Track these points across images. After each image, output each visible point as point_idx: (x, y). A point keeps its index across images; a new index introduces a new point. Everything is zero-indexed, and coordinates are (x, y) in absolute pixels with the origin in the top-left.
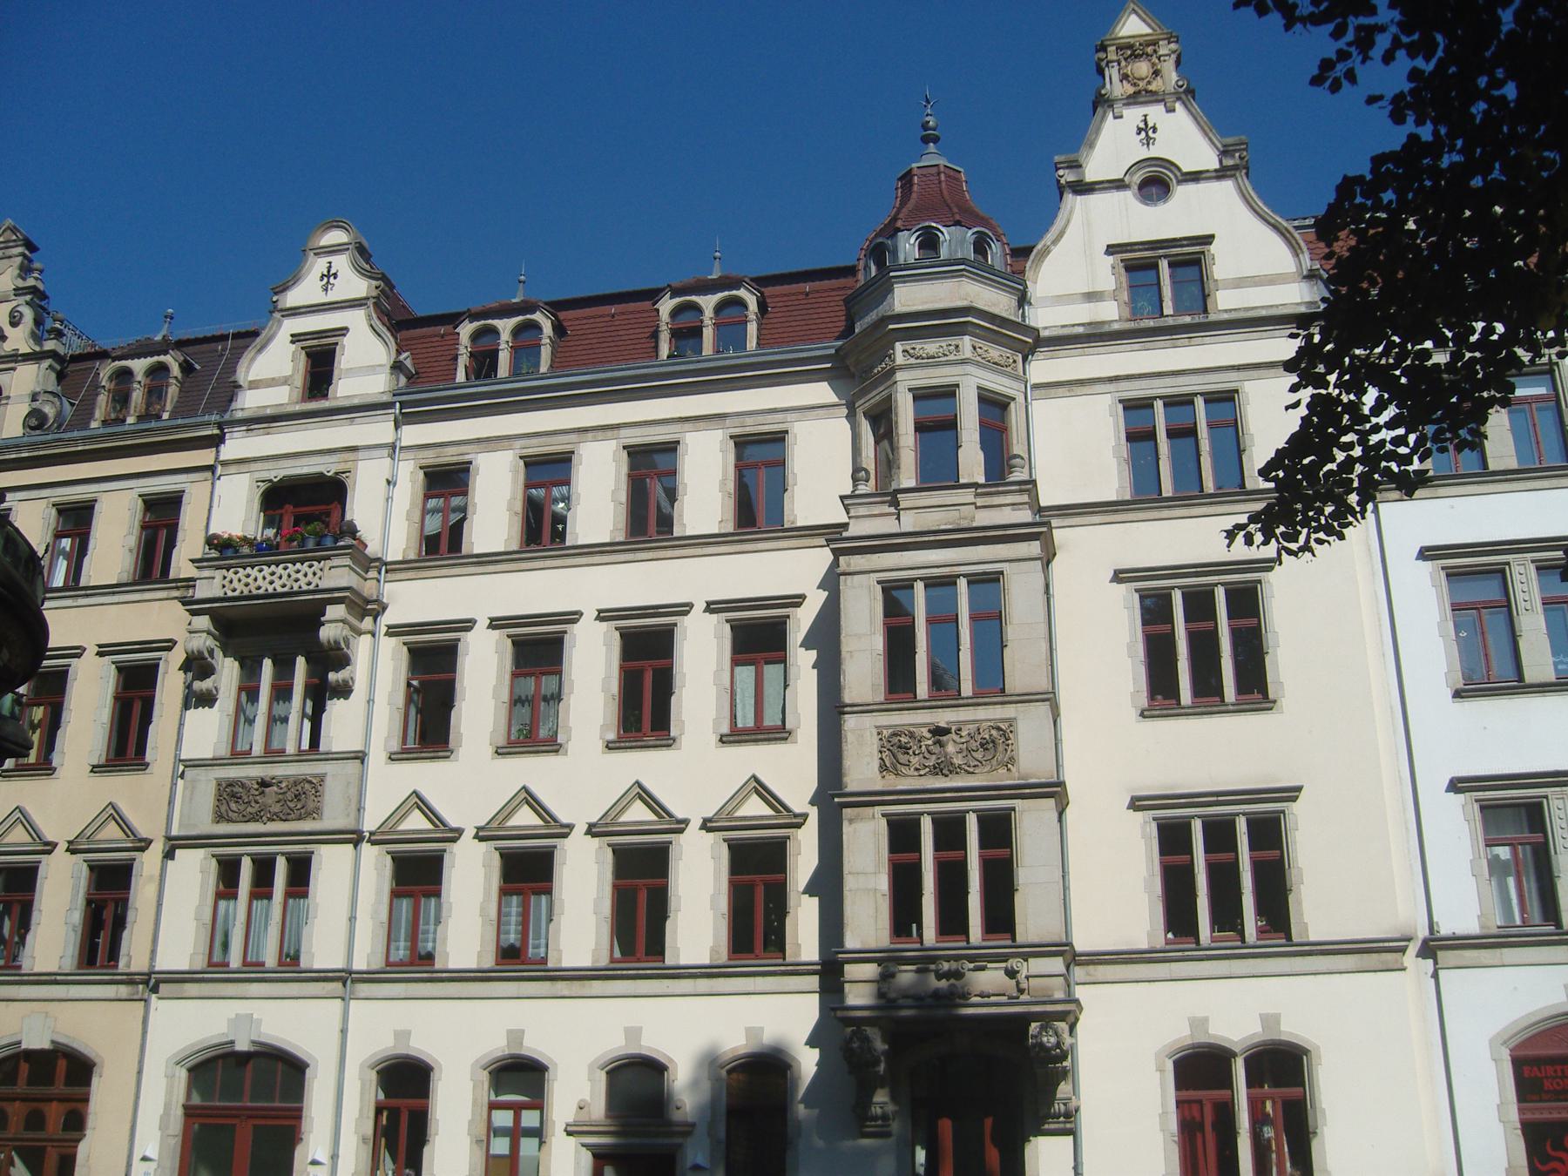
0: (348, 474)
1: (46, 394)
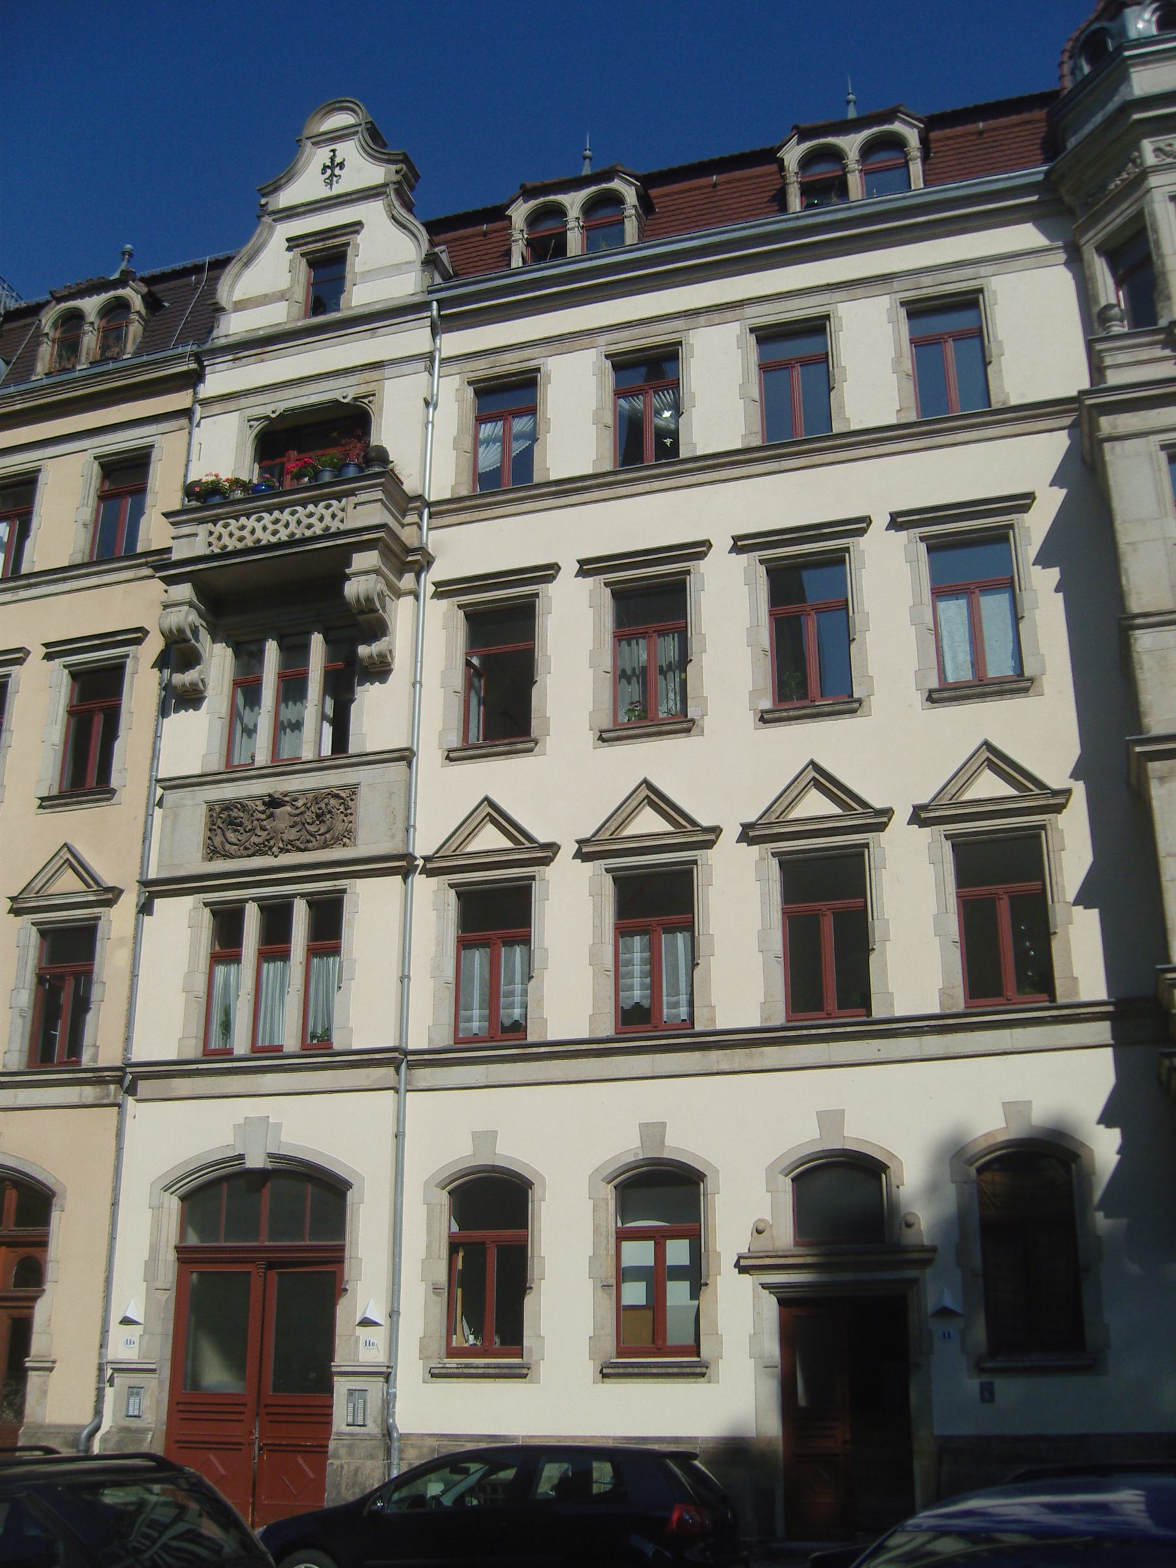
0: (371, 398)
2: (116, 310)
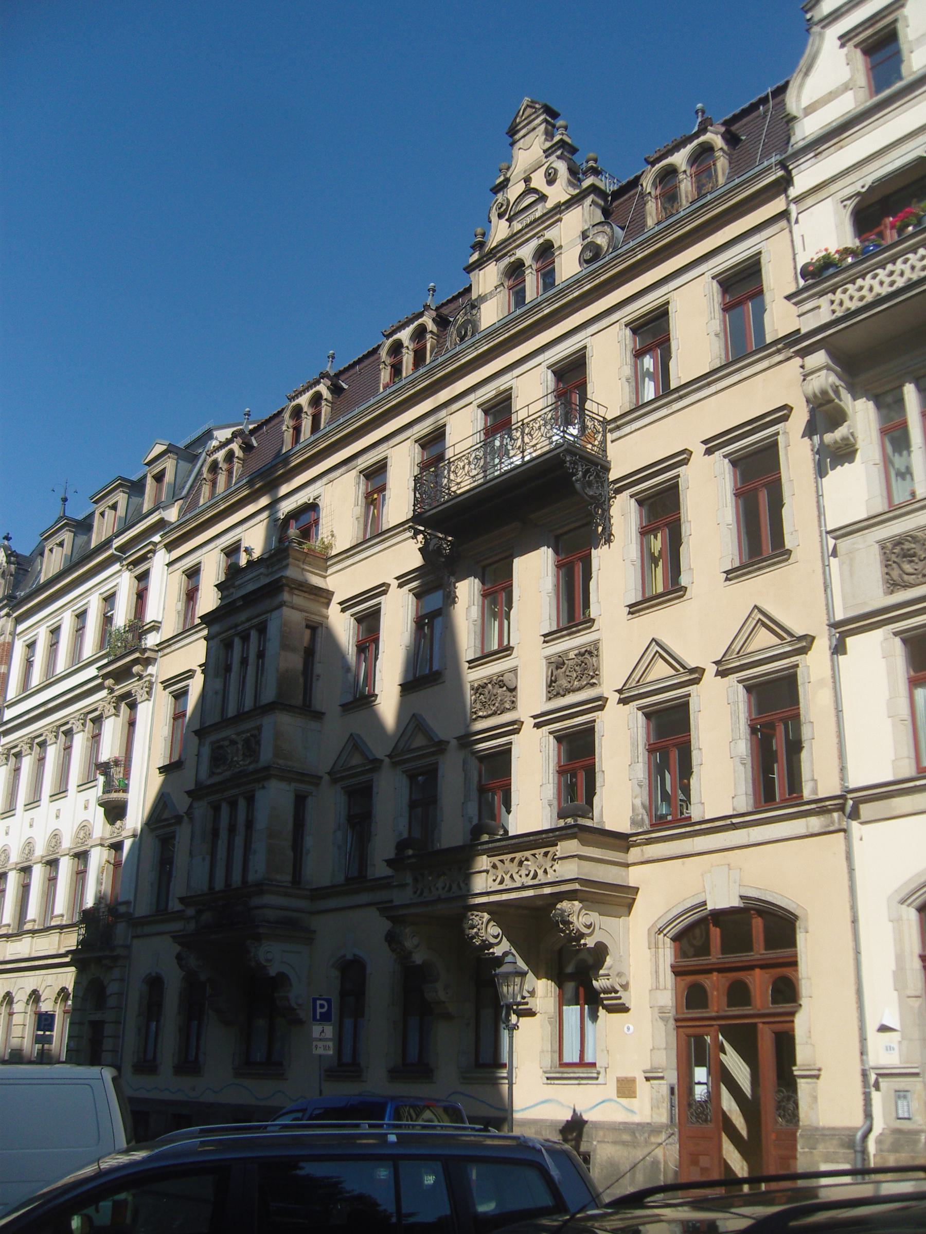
1: (596, 227)
2: (420, 332)
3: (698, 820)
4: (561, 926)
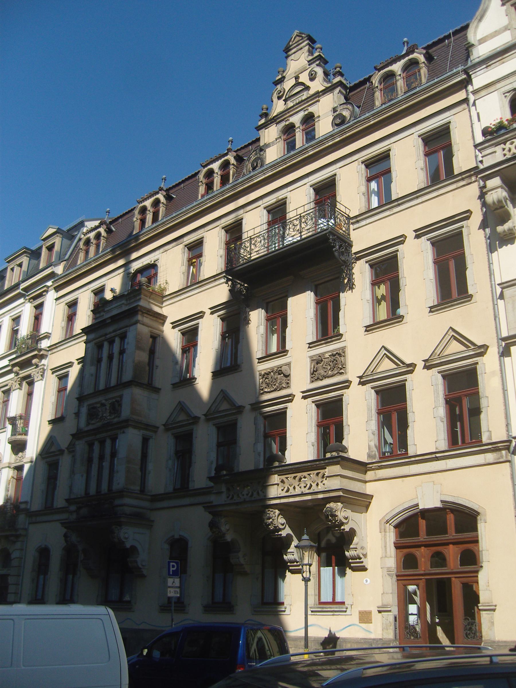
2: (226, 165)
3: (413, 455)
4: (330, 518)
